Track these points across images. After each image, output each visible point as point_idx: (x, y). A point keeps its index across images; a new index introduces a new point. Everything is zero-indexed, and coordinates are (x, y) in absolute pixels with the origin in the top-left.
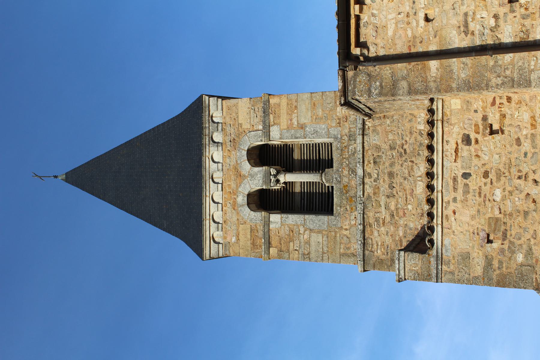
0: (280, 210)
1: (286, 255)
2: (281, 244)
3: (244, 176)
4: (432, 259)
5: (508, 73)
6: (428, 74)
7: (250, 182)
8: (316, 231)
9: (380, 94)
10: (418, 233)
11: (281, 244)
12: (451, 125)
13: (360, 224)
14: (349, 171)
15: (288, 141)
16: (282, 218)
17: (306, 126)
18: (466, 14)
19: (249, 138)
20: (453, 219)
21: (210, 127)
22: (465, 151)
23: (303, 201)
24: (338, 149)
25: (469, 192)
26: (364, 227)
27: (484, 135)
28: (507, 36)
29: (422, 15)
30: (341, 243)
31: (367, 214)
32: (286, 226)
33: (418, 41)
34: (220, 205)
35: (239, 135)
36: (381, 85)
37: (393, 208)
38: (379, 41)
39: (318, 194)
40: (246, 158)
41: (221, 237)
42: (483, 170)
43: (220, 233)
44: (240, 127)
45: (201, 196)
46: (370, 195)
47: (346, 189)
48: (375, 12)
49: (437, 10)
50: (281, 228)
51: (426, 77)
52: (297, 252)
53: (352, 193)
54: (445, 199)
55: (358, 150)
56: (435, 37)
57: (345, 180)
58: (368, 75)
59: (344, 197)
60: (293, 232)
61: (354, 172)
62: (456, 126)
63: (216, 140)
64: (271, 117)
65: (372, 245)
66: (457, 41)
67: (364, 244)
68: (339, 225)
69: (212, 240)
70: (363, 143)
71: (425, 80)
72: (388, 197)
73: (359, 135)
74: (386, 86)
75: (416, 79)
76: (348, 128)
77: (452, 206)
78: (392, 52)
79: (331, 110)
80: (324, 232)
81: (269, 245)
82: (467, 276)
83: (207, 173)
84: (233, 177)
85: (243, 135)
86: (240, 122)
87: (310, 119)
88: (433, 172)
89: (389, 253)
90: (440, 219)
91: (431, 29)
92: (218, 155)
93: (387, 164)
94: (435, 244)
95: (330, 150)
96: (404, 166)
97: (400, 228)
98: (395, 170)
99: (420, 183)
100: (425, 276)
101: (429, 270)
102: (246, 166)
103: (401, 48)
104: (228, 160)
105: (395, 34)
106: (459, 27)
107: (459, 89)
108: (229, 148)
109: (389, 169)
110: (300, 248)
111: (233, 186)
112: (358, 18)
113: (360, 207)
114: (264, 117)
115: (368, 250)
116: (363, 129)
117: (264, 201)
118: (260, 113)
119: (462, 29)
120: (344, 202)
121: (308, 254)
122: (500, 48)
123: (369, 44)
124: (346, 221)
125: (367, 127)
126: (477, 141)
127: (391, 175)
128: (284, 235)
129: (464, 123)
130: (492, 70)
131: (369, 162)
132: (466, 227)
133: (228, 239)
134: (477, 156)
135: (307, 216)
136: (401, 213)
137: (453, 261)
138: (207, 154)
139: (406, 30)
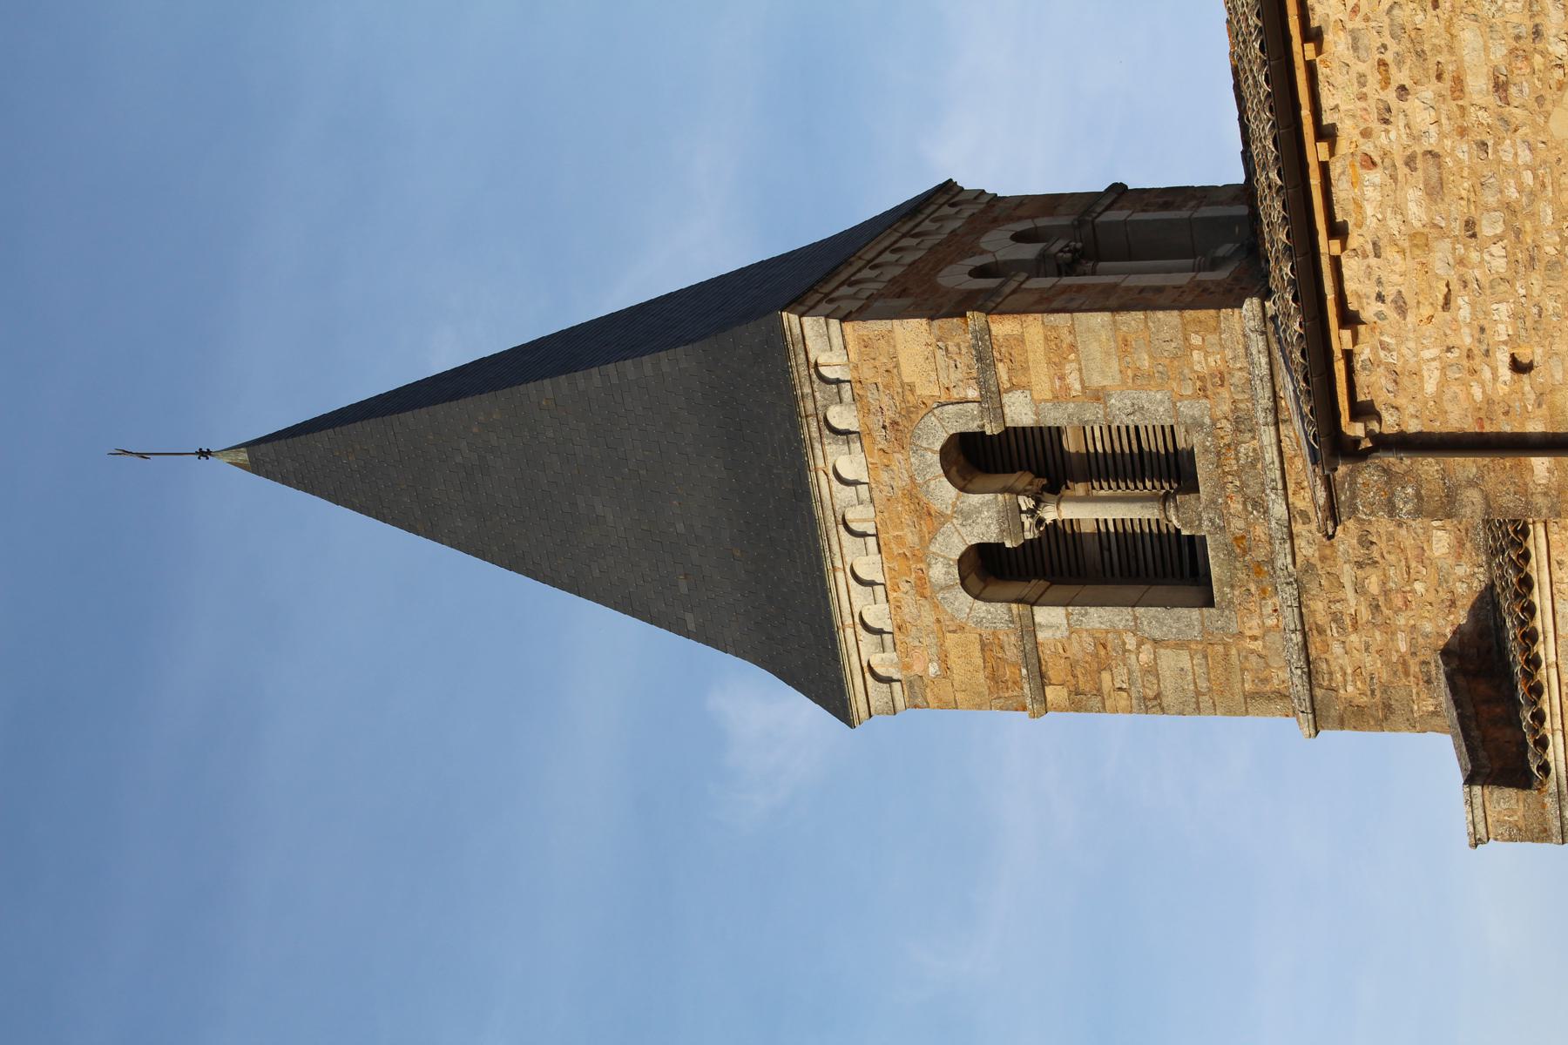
1: (1096, 702)
2: (1074, 676)
3: (942, 514)
4: (1548, 800)
7: (962, 530)
8: (1172, 643)
10: (1447, 645)
11: (1074, 676)
14: (1244, 504)
15: (1052, 418)
16: (1068, 615)
19: (940, 420)
23: (1106, 554)
24: (1206, 450)
26: (1304, 635)
29: (1503, 358)
30: (1243, 670)
31: (1307, 606)
32: (1084, 635)
33: (1499, 410)
34: (879, 590)
35: (908, 413)
37: (1373, 586)
38: (1401, 401)
39: (1148, 538)
40: (938, 470)
43: (891, 655)
44: (907, 393)
45: (822, 571)
46: (1312, 561)
48: (1386, 339)
50: (1069, 638)
51: (1526, 484)
52: (1124, 694)
53: (1260, 554)
55: (1268, 460)
56: (1540, 405)
57: (1237, 525)
58: (1384, 470)
59: (1238, 565)
61: (1259, 505)
63: (841, 426)
64: (1002, 368)
65: (1331, 673)
67: (1309, 674)
68: (1234, 628)
69: (868, 675)
70: (1279, 441)
71: (1524, 491)
72: (1360, 565)
73: (1266, 424)
74: (1430, 497)
75: (1500, 487)
76: (1229, 402)
78: (1437, 427)
80: (1193, 646)
83: (829, 513)
84: (906, 518)
86: (906, 380)
87: (1118, 377)
88: (1534, 630)
90: (1558, 720)
91: (1527, 388)
92: (850, 463)
94: (1553, 771)
97: (1400, 635)
99: (1440, 533)
102: (944, 492)
103: (1457, 421)
104: (885, 476)
110: (1131, 682)
111: (911, 538)
112: (1348, 356)
113: (1290, 591)
114: (982, 371)
115: (1320, 686)
117: (987, 568)
118: (966, 359)
121: (1155, 698)
123: (1379, 406)
124: (1255, 621)
128: (1080, 655)
133: (917, 669)
136: (1398, 601)
138: (820, 463)
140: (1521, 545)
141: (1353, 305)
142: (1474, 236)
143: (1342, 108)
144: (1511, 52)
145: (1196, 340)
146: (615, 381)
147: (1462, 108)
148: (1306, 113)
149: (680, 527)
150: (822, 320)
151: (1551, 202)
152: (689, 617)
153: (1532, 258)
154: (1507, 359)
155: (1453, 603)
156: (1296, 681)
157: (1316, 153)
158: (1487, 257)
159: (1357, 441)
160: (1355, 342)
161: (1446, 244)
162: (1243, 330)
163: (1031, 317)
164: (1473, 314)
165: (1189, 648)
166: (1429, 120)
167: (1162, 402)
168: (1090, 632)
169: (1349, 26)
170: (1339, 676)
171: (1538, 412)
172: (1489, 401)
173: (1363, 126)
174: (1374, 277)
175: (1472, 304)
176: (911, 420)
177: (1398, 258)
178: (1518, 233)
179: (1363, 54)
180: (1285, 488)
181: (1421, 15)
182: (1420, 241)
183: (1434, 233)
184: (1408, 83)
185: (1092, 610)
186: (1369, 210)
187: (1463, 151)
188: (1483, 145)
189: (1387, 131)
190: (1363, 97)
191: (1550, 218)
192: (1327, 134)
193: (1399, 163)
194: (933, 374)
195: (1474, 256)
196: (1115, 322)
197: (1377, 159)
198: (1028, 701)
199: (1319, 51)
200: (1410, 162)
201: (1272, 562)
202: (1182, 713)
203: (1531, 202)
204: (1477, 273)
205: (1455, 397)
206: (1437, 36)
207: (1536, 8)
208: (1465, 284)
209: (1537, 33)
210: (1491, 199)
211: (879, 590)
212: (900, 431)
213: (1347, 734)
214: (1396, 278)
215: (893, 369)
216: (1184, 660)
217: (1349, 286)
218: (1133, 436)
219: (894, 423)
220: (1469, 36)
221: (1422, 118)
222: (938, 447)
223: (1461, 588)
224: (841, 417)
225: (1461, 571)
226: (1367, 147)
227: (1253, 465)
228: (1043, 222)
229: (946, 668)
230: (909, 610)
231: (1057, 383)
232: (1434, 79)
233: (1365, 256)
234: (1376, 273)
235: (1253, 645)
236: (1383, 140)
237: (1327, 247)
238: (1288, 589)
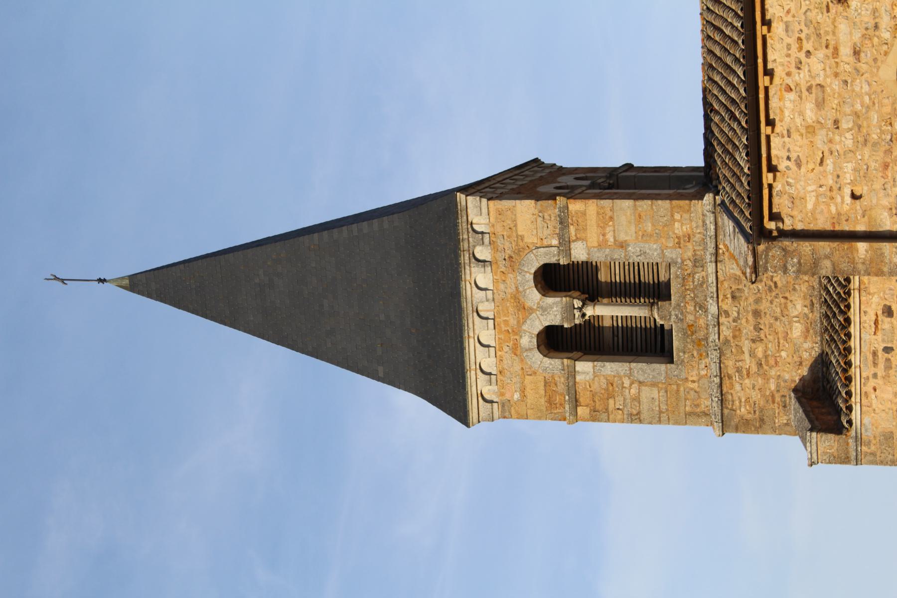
0: (580, 350)
1: (604, 416)
2: (594, 401)
3: (531, 309)
4: (850, 441)
6: (855, 255)
7: (541, 318)
9: (799, 271)
11: (594, 401)
12: (869, 294)
13: (716, 376)
14: (695, 307)
15: (598, 257)
16: (594, 367)
17: (629, 245)
20: (873, 396)
21: (471, 239)
23: (616, 338)
24: (677, 277)
25: (891, 368)
26: (721, 379)
29: (847, 192)
30: (686, 399)
32: (602, 378)
33: (843, 218)
34: (492, 350)
35: (519, 252)
36: (799, 262)
37: (760, 353)
38: (795, 213)
40: (532, 283)
41: (494, 393)
43: (494, 388)
44: (520, 241)
46: (729, 338)
47: (691, 329)
48: (790, 180)
49: (865, 188)
52: (620, 412)
53: (701, 334)
54: (864, 375)
57: (690, 318)
58: (783, 249)
59: (689, 340)
60: (612, 385)
61: (703, 308)
62: (876, 296)
64: (572, 229)
65: (733, 401)
66: (888, 223)
68: (683, 376)
69: (480, 399)
70: (717, 272)
71: (852, 261)
72: (753, 341)
73: (711, 262)
74: (805, 264)
77: (872, 383)
78: (812, 227)
79: (666, 225)
80: (660, 385)
81: (576, 403)
82: (890, 457)
83: (470, 305)
84: (511, 310)
85: (526, 252)
86: (520, 233)
87: (634, 235)
89: (757, 412)
91: (858, 207)
92: (483, 277)
93: (751, 300)
95: (655, 271)
96: (775, 303)
97: (772, 381)
98: (762, 308)
100: (844, 459)
101: (847, 452)
102: (534, 296)
103: (822, 224)
104: (502, 286)
105: (815, 208)
106: (891, 209)
108: (503, 269)
109: (754, 307)
110: (625, 405)
111: (513, 321)
112: (770, 187)
113: (715, 355)
114: (562, 229)
115: (727, 408)
116: (716, 254)
117: (554, 341)
118: (554, 223)
120: (689, 346)
123: (783, 215)
124: (693, 371)
125: (721, 251)
127: (757, 314)
129: (884, 292)
131: (725, 296)
132: (889, 405)
133: (508, 396)
135: (633, 365)
136: (772, 362)
137: (874, 442)
138: (468, 277)
140: (846, 300)
141: (774, 162)
142: (838, 128)
143: (778, 61)
144: (863, 36)
145: (677, 216)
146: (355, 233)
147: (837, 63)
148: (760, 61)
149: (382, 317)
150: (478, 198)
151: (877, 112)
152: (381, 369)
153: (866, 140)
154: (849, 192)
155: (801, 364)
156: (714, 404)
157: (763, 81)
158: (843, 139)
159: (771, 231)
160: (774, 180)
161: (824, 132)
162: (703, 212)
163: (591, 201)
164: (834, 168)
165: (658, 386)
166: (820, 68)
167: (656, 250)
168: (605, 377)
169: (785, 19)
170: (737, 403)
171: (863, 220)
172: (839, 214)
173: (787, 70)
174: (786, 148)
175: (834, 163)
176: (520, 256)
177: (799, 138)
178: (859, 127)
179: (790, 33)
180: (718, 297)
181: (820, 15)
182: (811, 130)
183: (818, 126)
184: (811, 49)
185: (607, 364)
186: (787, 113)
187: (836, 85)
188: (846, 82)
189: (799, 74)
190: (788, 56)
191: (876, 120)
192: (769, 73)
193: (804, 90)
194: (535, 231)
195: (837, 138)
196: (635, 205)
197: (793, 87)
198: (568, 414)
199: (769, 31)
200: (809, 89)
201: (707, 339)
202: (650, 423)
203: (867, 112)
204: (838, 147)
205: (822, 211)
206: (828, 26)
207: (877, 14)
208: (831, 153)
209: (876, 27)
210: (848, 110)
211: (492, 350)
212: (513, 262)
213: (740, 436)
214: (798, 149)
215: (513, 228)
216: (655, 393)
217: (774, 152)
218: (636, 268)
219: (511, 257)
220: (843, 27)
222: (533, 271)
223: (805, 355)
224: (482, 253)
225: (806, 345)
226: (789, 81)
227: (701, 285)
228: (588, 175)
229: (524, 395)
230: (507, 362)
231: (601, 237)
232: (824, 48)
233: (783, 137)
234: (788, 145)
235: (691, 385)
236: (797, 78)
237: (765, 130)
238: (715, 353)
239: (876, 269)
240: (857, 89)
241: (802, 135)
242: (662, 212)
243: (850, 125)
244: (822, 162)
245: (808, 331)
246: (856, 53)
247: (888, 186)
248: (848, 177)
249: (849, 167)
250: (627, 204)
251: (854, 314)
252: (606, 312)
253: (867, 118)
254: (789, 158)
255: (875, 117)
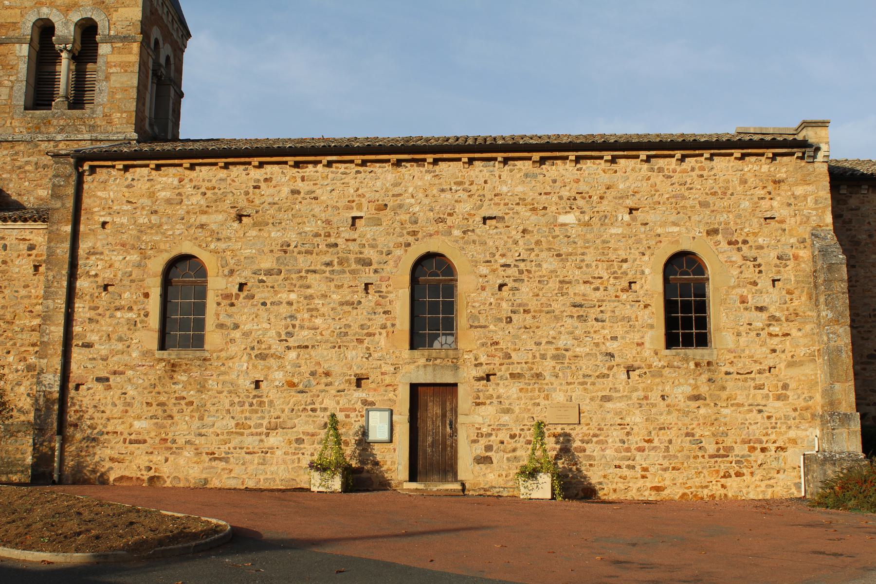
5: (55, 284)
15: (100, 61)
18: (102, 253)
22: (23, 246)
24: (84, 114)
27: (34, 261)
28: (82, 284)
29: (108, 219)
35: (107, 8)
36: (61, 186)
37: (28, 168)
38: (95, 183)
42: (8, 260)
53: (43, 129)
57: (55, 122)
61: (62, 131)
64: (120, 45)
68: (15, 117)
71: (59, 222)
72: (36, 164)
78: (85, 195)
97: (9, 175)
102: (76, 17)
103: (86, 201)
105: (97, 197)
107: (49, 248)
112: (113, 167)
113: (28, 137)
114: (120, 37)
118: (125, 32)
119: (92, 250)
122: (72, 277)
123: (94, 176)
126: (30, 255)
130: (59, 271)
134: (19, 256)
136: (22, 176)
139: (99, 206)
141: (131, 170)
145: (124, 115)
148: (200, 161)
154: (107, 220)
155: (20, 195)
157: (186, 163)
159: (82, 167)
161: (150, 203)
172: (92, 213)
175: (127, 211)
178: (151, 228)
182: (152, 195)
183: (154, 200)
186: (164, 179)
187: (181, 212)
188: (183, 219)
190: (204, 180)
192: (192, 167)
193: (179, 191)
195: (145, 213)
199: (221, 167)
200: (180, 194)
209: (219, 239)
210: (164, 220)
216: (4, 97)
217: (138, 169)
220: (220, 217)
221: (194, 200)
223: (25, 198)
225: (32, 199)
226: (186, 180)
227: (77, 130)
228: (173, 67)
229: (7, 8)
239: (53, 237)
240: (177, 226)
241: (149, 189)
242: (128, 105)
243: (153, 222)
244: (128, 202)
245: (41, 200)
246: (202, 226)
247: (109, 246)
248: (117, 220)
249: (125, 220)
250: (135, 82)
251: (30, 225)
252: (64, 68)
253: (157, 233)
254: (133, 180)
255: (157, 238)
